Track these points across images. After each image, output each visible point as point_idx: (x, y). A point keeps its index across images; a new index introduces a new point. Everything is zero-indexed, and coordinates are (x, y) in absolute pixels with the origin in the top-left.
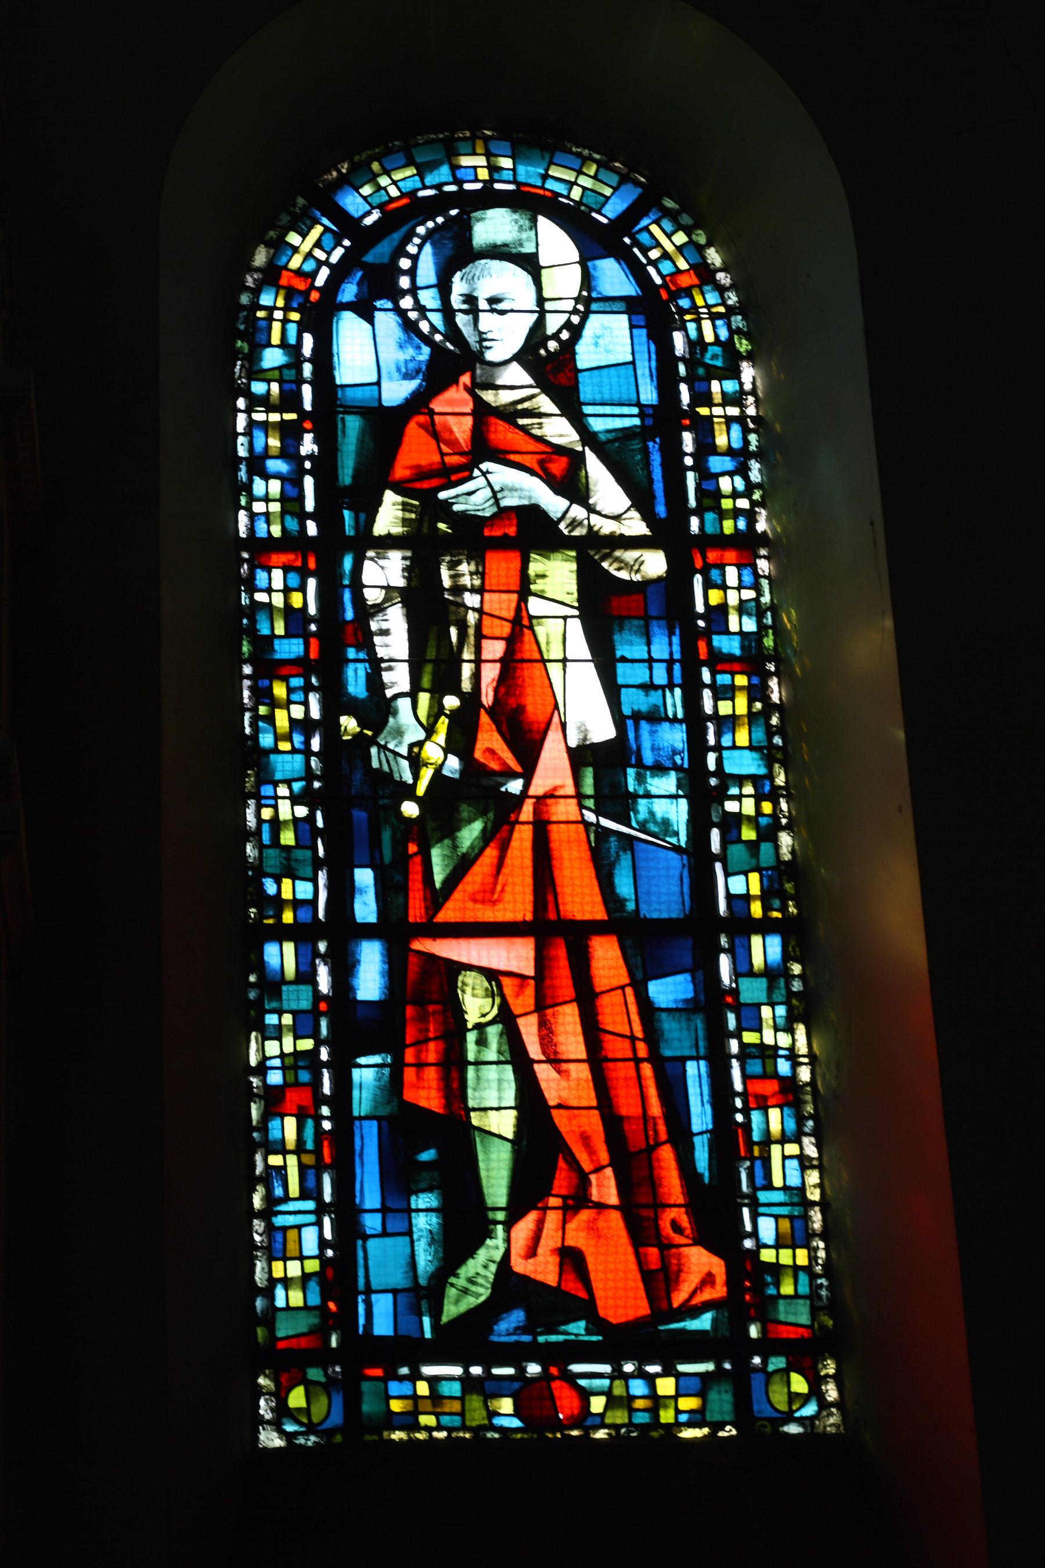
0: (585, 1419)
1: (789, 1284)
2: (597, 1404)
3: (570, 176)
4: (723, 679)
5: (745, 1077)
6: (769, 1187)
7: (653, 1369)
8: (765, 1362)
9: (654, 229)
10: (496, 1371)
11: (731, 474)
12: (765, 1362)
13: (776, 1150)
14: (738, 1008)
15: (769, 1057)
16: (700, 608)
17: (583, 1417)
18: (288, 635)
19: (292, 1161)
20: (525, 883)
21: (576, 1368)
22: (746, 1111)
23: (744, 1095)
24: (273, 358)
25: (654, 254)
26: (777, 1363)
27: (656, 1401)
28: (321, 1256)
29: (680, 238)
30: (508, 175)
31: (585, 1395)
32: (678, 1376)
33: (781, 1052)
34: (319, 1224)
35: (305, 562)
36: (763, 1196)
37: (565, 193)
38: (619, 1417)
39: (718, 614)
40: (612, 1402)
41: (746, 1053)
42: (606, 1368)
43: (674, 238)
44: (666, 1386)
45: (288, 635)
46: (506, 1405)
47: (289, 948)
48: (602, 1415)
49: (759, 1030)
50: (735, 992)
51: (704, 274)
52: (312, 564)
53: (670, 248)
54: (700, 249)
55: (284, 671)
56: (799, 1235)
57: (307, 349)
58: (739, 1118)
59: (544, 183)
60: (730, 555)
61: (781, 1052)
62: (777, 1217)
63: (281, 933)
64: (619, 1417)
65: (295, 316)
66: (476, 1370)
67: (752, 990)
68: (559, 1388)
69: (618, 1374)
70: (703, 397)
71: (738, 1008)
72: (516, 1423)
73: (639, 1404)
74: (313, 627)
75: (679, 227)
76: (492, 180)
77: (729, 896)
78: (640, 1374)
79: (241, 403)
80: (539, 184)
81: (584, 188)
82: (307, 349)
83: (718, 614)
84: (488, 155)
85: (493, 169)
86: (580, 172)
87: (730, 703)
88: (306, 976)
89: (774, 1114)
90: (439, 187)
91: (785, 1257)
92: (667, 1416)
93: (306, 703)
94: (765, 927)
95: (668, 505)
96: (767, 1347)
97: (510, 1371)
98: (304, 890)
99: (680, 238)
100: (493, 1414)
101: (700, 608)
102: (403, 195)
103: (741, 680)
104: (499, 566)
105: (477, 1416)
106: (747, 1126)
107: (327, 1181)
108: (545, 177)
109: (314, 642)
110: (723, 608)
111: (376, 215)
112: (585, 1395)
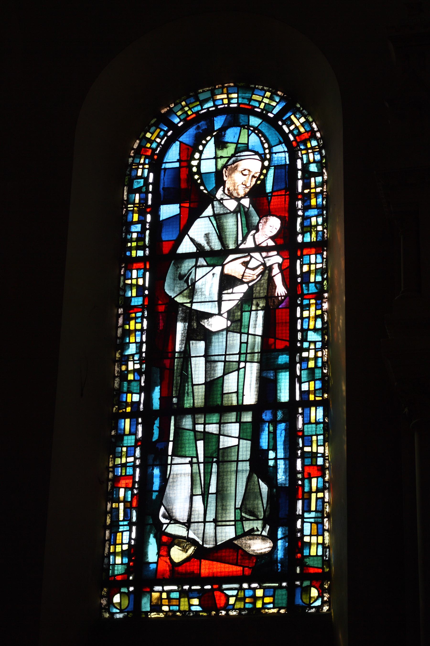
0: (227, 606)
1: (308, 549)
2: (232, 601)
3: (260, 99)
4: (306, 302)
5: (303, 465)
6: (310, 511)
7: (254, 585)
8: (302, 583)
9: (293, 117)
10: (193, 588)
11: (317, 216)
12: (302, 583)
13: (314, 496)
14: (303, 437)
15: (314, 457)
16: (299, 273)
17: (227, 607)
18: (137, 296)
19: (122, 505)
20: (284, 383)
21: (224, 586)
22: (303, 480)
23: (302, 472)
24: (138, 184)
25: (292, 127)
26: (306, 583)
27: (255, 598)
28: (129, 543)
29: (303, 120)
30: (235, 101)
31: (228, 597)
32: (265, 588)
33: (319, 455)
34: (130, 531)
35: (145, 266)
36: (306, 515)
37: (258, 105)
38: (240, 605)
39: (306, 276)
40: (238, 599)
41: (304, 455)
42: (236, 586)
43: (300, 120)
44: (259, 593)
45: (137, 296)
46: (195, 601)
47: (128, 421)
48: (234, 605)
49: (311, 446)
50: (303, 431)
51: (312, 133)
52: (148, 267)
53: (298, 124)
54: (310, 123)
55: (136, 310)
56: (320, 531)
57: (151, 180)
58: (300, 482)
59: (249, 103)
60: (313, 251)
61: (319, 455)
62: (311, 523)
63: (125, 416)
64: (240, 605)
65: (147, 166)
66: (186, 587)
67: (309, 429)
68: (217, 593)
69: (241, 589)
70: (306, 185)
71: (303, 437)
72: (199, 609)
73: (247, 600)
74: (147, 292)
75: (303, 115)
76: (229, 103)
77: (301, 392)
78: (250, 588)
79: (318, 135)
80: (248, 103)
81: (265, 103)
82: (151, 180)
83: (306, 276)
84: (228, 94)
85: (229, 99)
86: (263, 97)
87: (308, 312)
88: (133, 433)
89: (314, 481)
90: (208, 108)
91: (314, 539)
92: (259, 605)
93: (142, 323)
94: (316, 404)
95: (120, 279)
96: (302, 577)
97: (198, 587)
98: (136, 398)
99: (303, 120)
100: (190, 605)
101: (299, 273)
102: (193, 113)
103: (313, 301)
104: (268, 249)
105: (184, 606)
106: (303, 486)
107: (134, 513)
108: (250, 99)
109: (147, 299)
110: (309, 272)
111: (182, 123)
112: (228, 597)
